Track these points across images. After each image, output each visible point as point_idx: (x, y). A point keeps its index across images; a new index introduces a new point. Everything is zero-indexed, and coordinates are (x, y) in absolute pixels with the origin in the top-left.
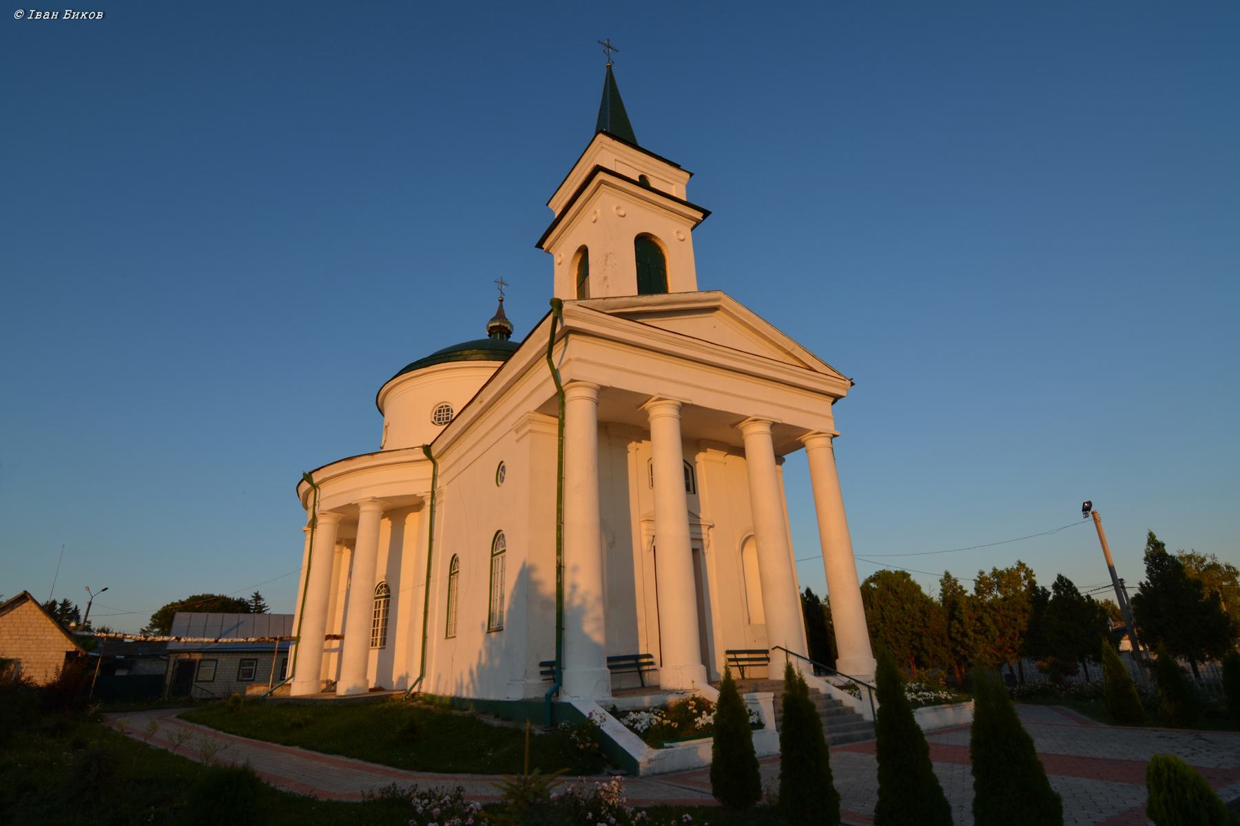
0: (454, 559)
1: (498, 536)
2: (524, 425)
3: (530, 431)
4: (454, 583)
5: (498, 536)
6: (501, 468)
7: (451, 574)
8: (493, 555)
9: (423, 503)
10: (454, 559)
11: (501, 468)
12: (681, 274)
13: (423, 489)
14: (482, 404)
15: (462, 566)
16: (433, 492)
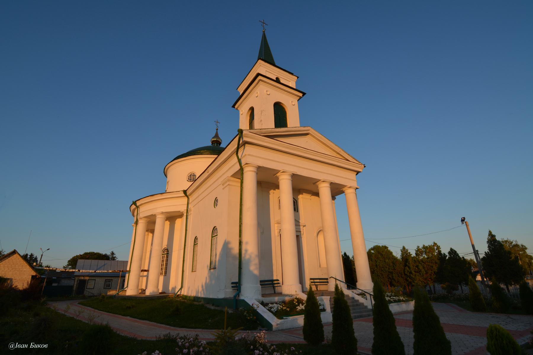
0: (196, 238)
1: (215, 229)
2: (226, 182)
3: (229, 185)
4: (196, 248)
5: (215, 229)
6: (216, 200)
7: (194, 245)
8: (212, 237)
9: (183, 214)
10: (196, 238)
11: (216, 200)
12: (293, 120)
13: (183, 209)
14: (209, 173)
15: (199, 241)
16: (187, 210)
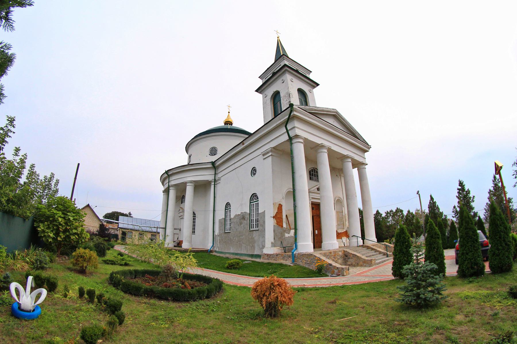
16: (215, 179)
